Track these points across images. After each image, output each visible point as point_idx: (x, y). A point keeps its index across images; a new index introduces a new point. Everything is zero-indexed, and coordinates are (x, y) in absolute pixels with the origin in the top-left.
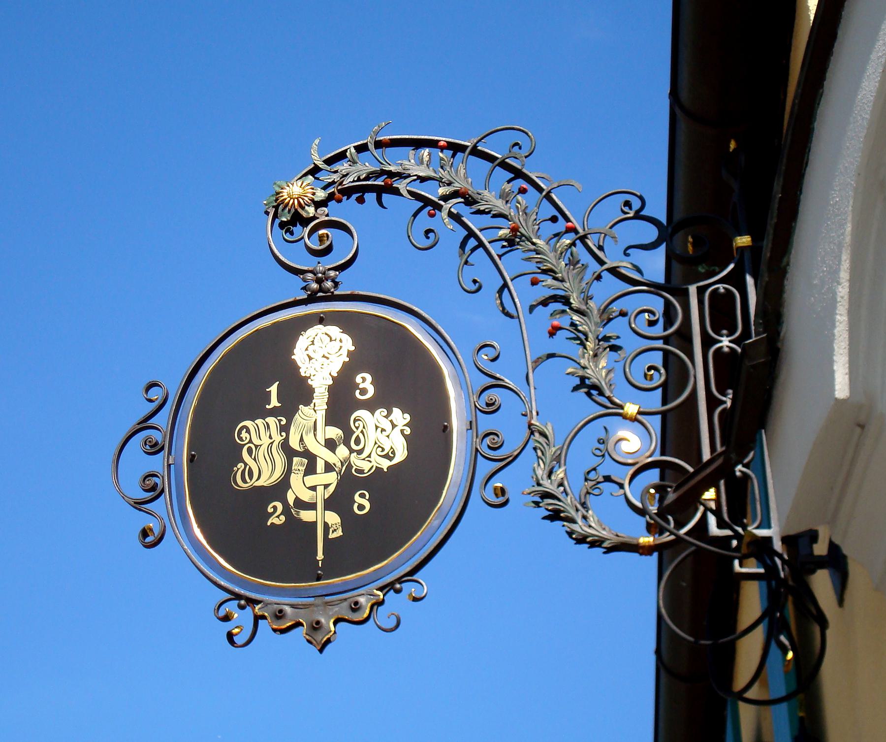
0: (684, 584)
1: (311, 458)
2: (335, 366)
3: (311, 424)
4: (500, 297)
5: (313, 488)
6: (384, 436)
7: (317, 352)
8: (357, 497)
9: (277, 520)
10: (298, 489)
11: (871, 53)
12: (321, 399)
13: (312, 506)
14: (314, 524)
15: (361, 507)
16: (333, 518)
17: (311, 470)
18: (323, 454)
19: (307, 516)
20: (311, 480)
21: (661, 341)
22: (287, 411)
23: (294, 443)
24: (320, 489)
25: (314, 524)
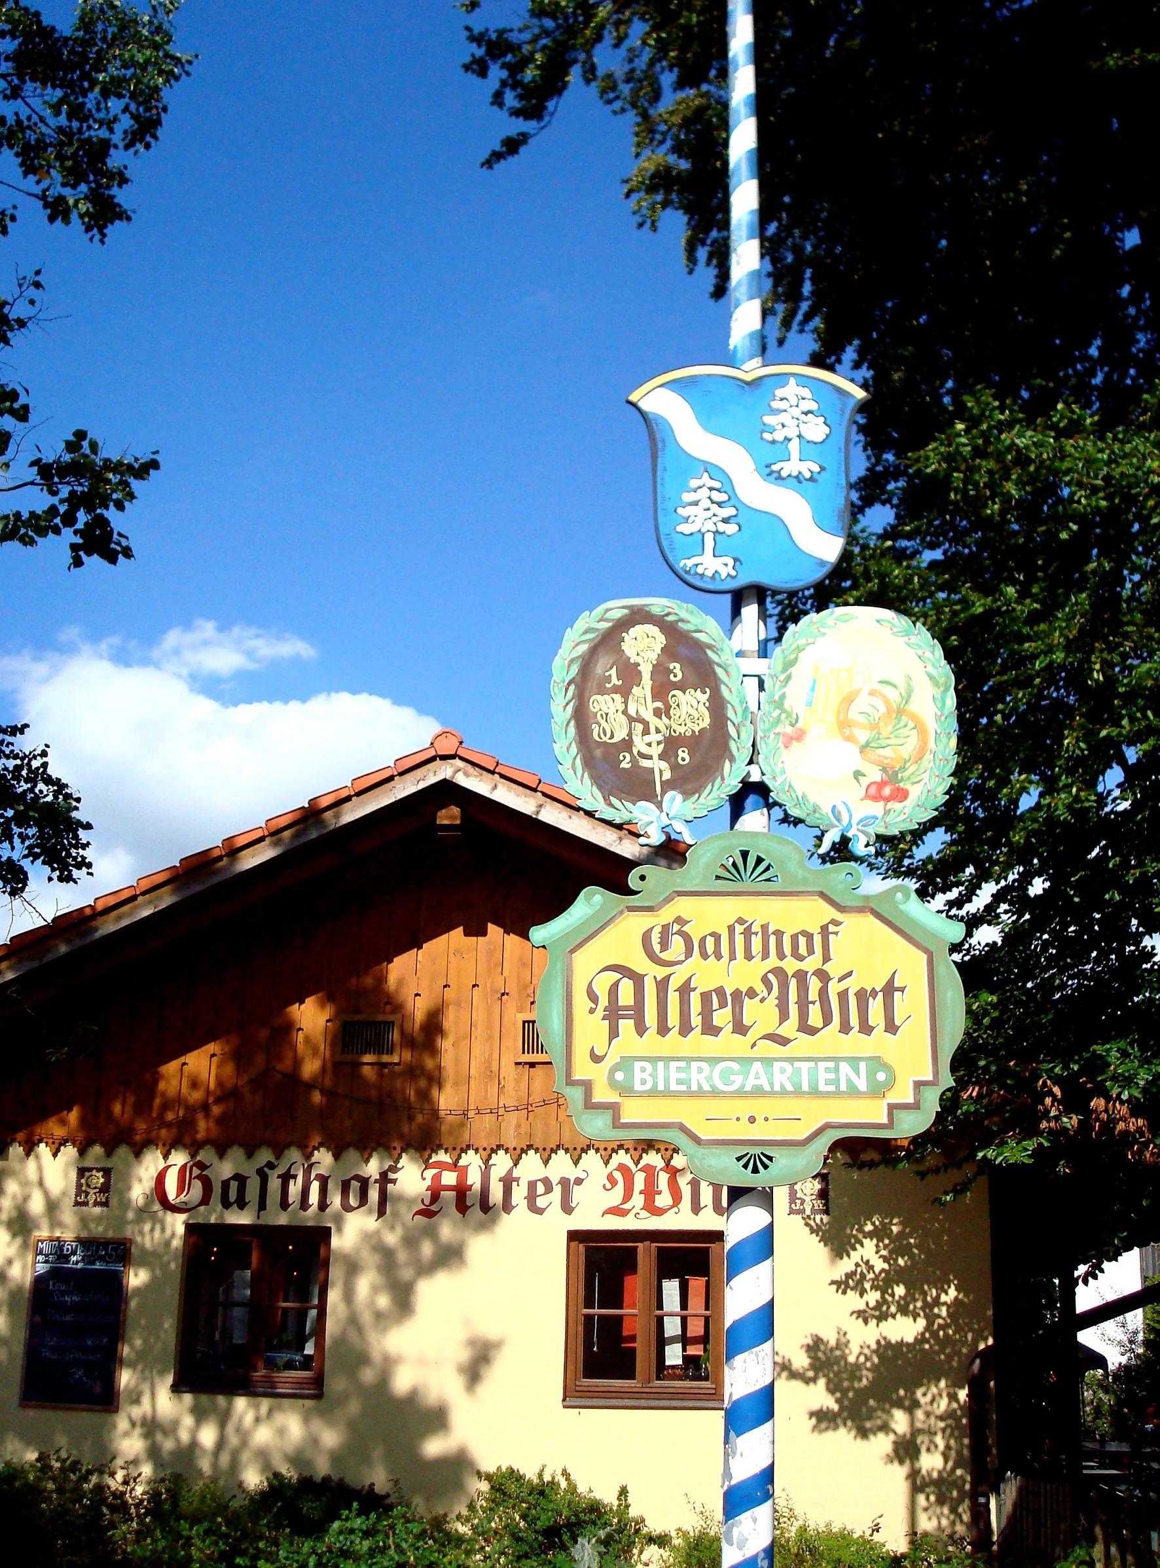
0: (1012, 1063)
1: (646, 724)
2: (653, 657)
3: (642, 699)
4: (567, 725)
5: (649, 745)
6: (691, 711)
7: (644, 643)
8: (680, 751)
9: (625, 765)
10: (639, 744)
11: (129, 1188)
12: (647, 681)
13: (650, 758)
14: (652, 771)
15: (683, 759)
16: (664, 765)
17: (646, 732)
18: (654, 722)
19: (645, 763)
20: (647, 739)
21: (940, 831)
22: (625, 691)
23: (632, 711)
24: (654, 745)
25: (652, 771)
